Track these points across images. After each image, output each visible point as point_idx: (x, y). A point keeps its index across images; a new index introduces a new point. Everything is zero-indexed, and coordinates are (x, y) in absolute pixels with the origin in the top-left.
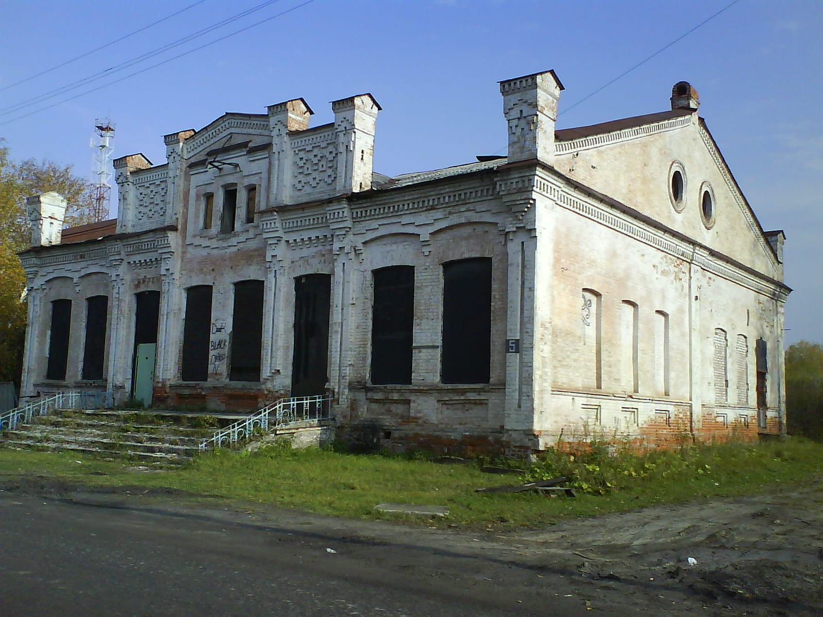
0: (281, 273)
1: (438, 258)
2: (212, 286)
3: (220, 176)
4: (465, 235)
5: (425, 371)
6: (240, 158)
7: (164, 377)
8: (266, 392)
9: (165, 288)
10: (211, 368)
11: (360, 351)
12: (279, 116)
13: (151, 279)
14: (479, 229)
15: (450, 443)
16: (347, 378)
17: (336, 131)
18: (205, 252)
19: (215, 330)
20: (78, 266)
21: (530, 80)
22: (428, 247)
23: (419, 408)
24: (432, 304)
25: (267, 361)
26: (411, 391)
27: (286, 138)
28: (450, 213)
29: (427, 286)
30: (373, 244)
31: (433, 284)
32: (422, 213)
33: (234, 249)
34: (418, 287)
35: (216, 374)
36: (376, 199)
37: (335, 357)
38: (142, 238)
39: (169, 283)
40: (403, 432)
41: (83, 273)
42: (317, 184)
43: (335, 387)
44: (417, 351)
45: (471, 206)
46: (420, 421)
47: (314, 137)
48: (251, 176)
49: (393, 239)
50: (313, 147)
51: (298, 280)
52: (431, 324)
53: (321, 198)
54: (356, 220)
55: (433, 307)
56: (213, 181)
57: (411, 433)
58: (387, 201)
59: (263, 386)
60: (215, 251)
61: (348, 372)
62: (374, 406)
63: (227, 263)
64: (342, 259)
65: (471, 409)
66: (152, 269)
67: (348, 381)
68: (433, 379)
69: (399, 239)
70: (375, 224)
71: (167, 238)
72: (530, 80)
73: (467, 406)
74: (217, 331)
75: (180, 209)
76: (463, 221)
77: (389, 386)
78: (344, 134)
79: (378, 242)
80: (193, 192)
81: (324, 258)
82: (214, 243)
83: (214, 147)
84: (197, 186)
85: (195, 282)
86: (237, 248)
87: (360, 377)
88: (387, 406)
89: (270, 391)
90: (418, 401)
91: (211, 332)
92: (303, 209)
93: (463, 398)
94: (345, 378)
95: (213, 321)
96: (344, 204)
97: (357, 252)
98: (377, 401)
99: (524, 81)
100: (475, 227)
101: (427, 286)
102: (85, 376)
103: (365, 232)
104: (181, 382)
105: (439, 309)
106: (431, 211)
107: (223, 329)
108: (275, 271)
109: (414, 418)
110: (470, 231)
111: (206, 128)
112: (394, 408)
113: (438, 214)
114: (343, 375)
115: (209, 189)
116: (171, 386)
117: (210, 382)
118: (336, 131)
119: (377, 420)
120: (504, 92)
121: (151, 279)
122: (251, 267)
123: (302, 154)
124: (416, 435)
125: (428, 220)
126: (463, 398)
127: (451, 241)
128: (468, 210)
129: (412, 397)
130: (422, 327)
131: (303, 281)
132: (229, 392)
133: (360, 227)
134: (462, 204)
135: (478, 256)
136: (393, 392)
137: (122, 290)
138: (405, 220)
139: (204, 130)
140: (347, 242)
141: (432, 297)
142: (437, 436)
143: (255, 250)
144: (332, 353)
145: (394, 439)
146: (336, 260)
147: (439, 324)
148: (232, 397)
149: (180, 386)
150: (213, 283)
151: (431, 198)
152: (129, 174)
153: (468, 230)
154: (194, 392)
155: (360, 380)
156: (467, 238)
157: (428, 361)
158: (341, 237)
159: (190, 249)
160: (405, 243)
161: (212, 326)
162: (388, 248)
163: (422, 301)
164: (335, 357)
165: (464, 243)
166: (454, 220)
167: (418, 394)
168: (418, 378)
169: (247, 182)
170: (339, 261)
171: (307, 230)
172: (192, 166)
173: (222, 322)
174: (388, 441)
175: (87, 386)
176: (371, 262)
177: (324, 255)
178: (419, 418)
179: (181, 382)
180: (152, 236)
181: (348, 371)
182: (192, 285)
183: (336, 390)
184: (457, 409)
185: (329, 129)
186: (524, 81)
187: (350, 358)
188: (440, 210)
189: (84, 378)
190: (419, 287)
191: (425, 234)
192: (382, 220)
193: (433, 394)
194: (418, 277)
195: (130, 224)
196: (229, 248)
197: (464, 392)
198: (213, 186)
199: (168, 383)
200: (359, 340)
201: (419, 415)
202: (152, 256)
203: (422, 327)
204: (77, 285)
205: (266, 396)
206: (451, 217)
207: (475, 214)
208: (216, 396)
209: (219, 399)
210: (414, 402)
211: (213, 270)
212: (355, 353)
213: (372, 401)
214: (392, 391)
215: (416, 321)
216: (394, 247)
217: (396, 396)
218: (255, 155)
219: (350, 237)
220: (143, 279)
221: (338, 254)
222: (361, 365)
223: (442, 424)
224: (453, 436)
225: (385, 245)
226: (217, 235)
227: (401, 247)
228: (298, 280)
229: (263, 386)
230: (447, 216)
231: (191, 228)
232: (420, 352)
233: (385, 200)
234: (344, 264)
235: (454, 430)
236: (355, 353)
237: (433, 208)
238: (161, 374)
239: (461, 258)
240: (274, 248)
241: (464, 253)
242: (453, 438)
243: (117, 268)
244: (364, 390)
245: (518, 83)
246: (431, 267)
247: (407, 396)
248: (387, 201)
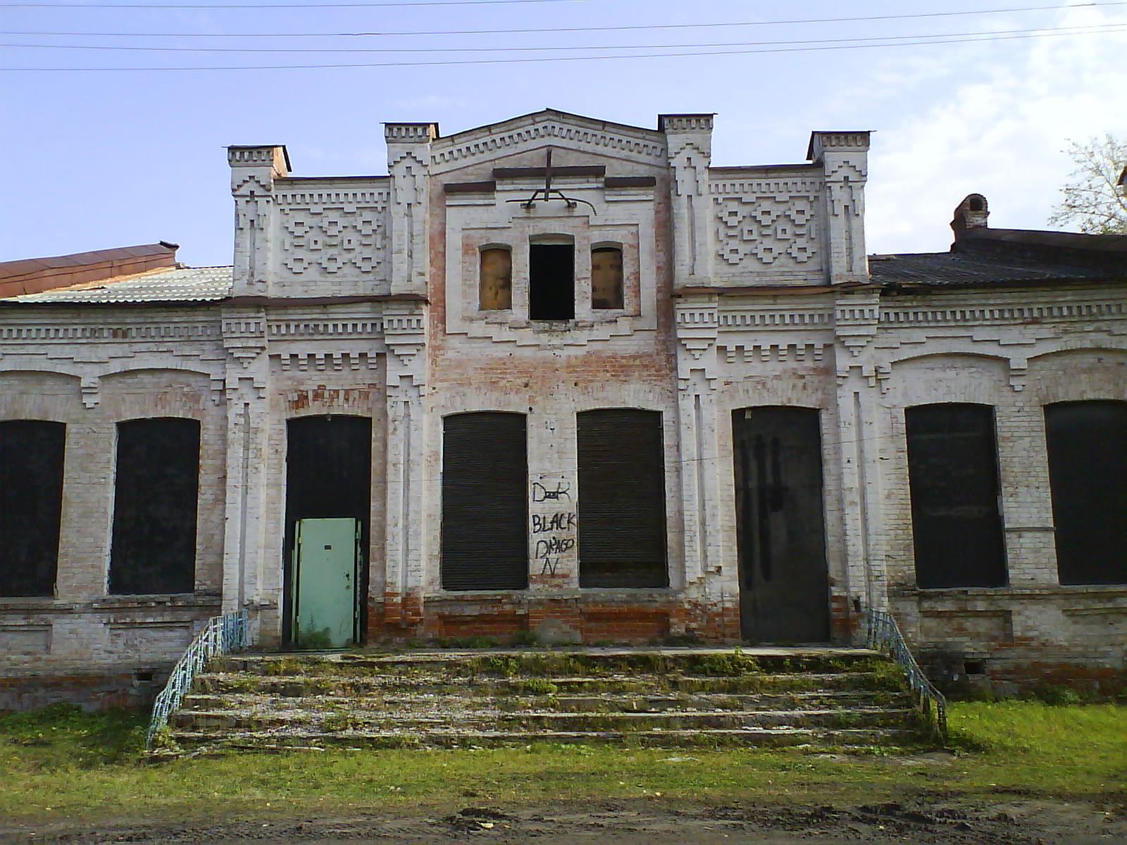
0: (711, 401)
1: (1037, 396)
2: (524, 416)
3: (528, 218)
4: (1085, 366)
5: (1034, 566)
6: (584, 193)
7: (411, 583)
8: (687, 606)
9: (395, 410)
10: (536, 566)
11: (896, 535)
12: (689, 136)
13: (342, 394)
14: (1109, 360)
15: (1103, 674)
16: (885, 579)
17: (827, 179)
18: (501, 352)
19: (540, 495)
20: (102, 352)
21: (420, 130)
22: (1022, 378)
23: (1030, 623)
24: (1035, 464)
25: (695, 551)
26: (1013, 597)
27: (706, 175)
28: (1066, 332)
29: (1021, 437)
30: (906, 366)
31: (1033, 434)
32: (1012, 327)
33: (581, 352)
34: (1005, 439)
35: (553, 575)
36: (934, 298)
37: (854, 545)
38: (332, 310)
39: (406, 403)
40: (1010, 661)
41: (115, 367)
42: (774, 258)
43: (860, 594)
44: (1014, 535)
45: (1104, 326)
46: (1034, 643)
47: (763, 182)
48: (609, 228)
49: (948, 362)
50: (757, 198)
51: (738, 415)
52: (1037, 494)
53: (786, 283)
54: (885, 326)
55: (1038, 469)
56: (510, 225)
57: (1025, 662)
58: (951, 303)
59: (682, 596)
60: (528, 352)
61: (885, 568)
62: (930, 623)
63: (563, 374)
64: (853, 385)
65: (1120, 622)
66: (341, 373)
67: (886, 582)
68: (1051, 579)
69: (959, 362)
70: (919, 335)
71: (419, 318)
72: (420, 130)
73: (1112, 618)
74: (545, 497)
75: (423, 260)
76: (1088, 345)
77: (972, 591)
78: (841, 187)
79: (918, 364)
80: (454, 240)
81: (803, 381)
82: (527, 336)
83: (507, 164)
84: (463, 229)
85: (477, 402)
86: (586, 349)
87: (902, 577)
88: (955, 622)
89: (696, 605)
90: (1027, 613)
91: (530, 500)
92: (775, 297)
93: (1110, 605)
94: (880, 578)
95: (532, 478)
96: (876, 299)
97: (879, 376)
98: (939, 615)
99: (404, 129)
100: (1102, 355)
101: (1021, 437)
102: (116, 585)
103: (899, 345)
104: (444, 593)
105: (1042, 473)
106: (1030, 326)
107: (564, 492)
108: (697, 396)
109: (1019, 638)
110: (1092, 360)
111: (489, 127)
112: (969, 624)
113: (1045, 332)
114: (877, 573)
115: (498, 239)
116: (428, 601)
117: (536, 591)
118: (827, 179)
119: (947, 644)
120: (389, 140)
121: (342, 394)
122: (626, 386)
123: (734, 206)
124: (1036, 666)
125: (1024, 337)
126: (1110, 605)
127: (1060, 373)
128: (1098, 330)
129: (1015, 607)
130: (1020, 499)
131: (748, 416)
132: (591, 608)
133: (893, 338)
134: (1089, 321)
135: (1112, 398)
136: (976, 600)
137: (256, 407)
138: (979, 334)
139: (484, 129)
140: (867, 359)
141: (1033, 454)
142: (1077, 665)
143: (635, 357)
144: (848, 538)
145: (993, 672)
146: (840, 385)
147: (1047, 495)
148: (593, 617)
149: (443, 601)
150: (531, 409)
151: (1035, 307)
152: (272, 181)
153: (1090, 359)
154: (495, 611)
155: (903, 582)
156: (1090, 370)
157: (1036, 551)
158: (697, 354)
159: (454, 342)
160: (973, 370)
161: (530, 487)
162: (939, 374)
163: (1016, 460)
164: (854, 545)
165: (1083, 376)
166: (1073, 342)
167: (1025, 601)
168: (1021, 576)
169: (597, 237)
170: (846, 388)
171: (771, 333)
172: (450, 189)
173: (561, 480)
174: (983, 678)
175: (124, 609)
176: (905, 394)
177: (803, 377)
178: (1032, 639)
179: (444, 593)
180: (368, 309)
181: (882, 567)
182: (468, 410)
183: (863, 599)
184: (1092, 623)
185: (799, 174)
186: (404, 129)
187: (881, 546)
188: (1046, 326)
189: (112, 590)
190: (1008, 438)
191: (1018, 359)
192: (934, 330)
193: (1053, 602)
194: (1002, 423)
195: (271, 279)
196: (566, 347)
197: (1112, 597)
198: (505, 232)
199: (422, 595)
200: (892, 517)
201: (1031, 634)
202: (351, 349)
203: (1020, 499)
204: (91, 391)
205: (688, 613)
206: (1066, 338)
207: (1108, 337)
208: (557, 617)
209: (567, 622)
210: (1019, 614)
211: (526, 385)
212: (888, 538)
213: (926, 614)
214: (975, 597)
215: (1006, 490)
216: (951, 374)
217: (981, 606)
218: (623, 193)
219: (870, 350)
220: (314, 390)
221: (844, 377)
222: (904, 558)
223: (1076, 645)
224: (1108, 664)
225: (932, 369)
226: (528, 323)
227: (964, 374)
228: (738, 415)
229: (682, 596)
230: (1061, 335)
231: (455, 303)
232: (1020, 537)
233: (949, 300)
234: (857, 394)
235: (1105, 655)
236: (888, 538)
237: (1035, 321)
238: (400, 578)
239: (1080, 399)
240: (245, 365)
241: (1084, 392)
242: (1108, 666)
243: (245, 365)
244: (917, 598)
245: (395, 129)
246: (1026, 409)
247: (1004, 604)
248: (951, 303)
